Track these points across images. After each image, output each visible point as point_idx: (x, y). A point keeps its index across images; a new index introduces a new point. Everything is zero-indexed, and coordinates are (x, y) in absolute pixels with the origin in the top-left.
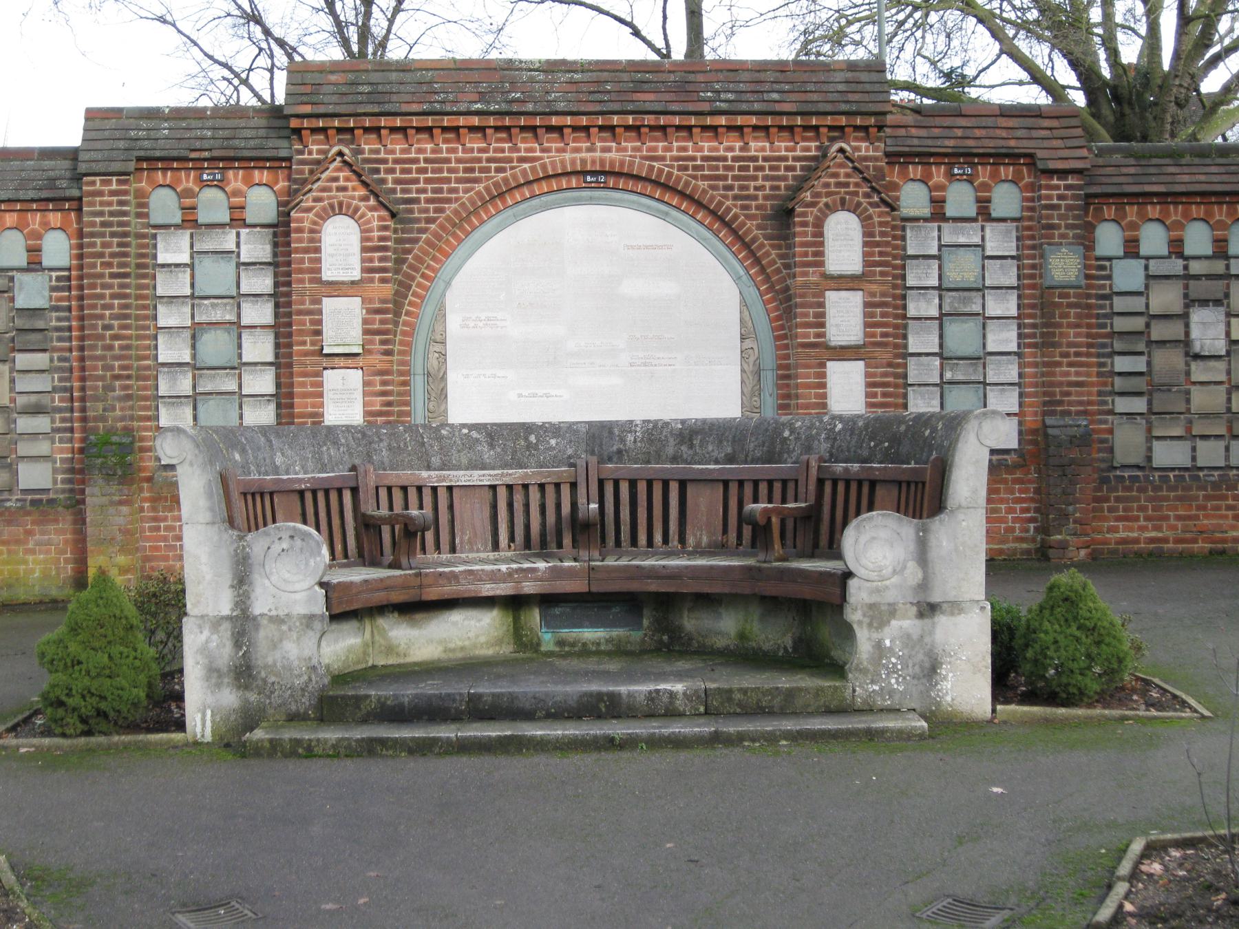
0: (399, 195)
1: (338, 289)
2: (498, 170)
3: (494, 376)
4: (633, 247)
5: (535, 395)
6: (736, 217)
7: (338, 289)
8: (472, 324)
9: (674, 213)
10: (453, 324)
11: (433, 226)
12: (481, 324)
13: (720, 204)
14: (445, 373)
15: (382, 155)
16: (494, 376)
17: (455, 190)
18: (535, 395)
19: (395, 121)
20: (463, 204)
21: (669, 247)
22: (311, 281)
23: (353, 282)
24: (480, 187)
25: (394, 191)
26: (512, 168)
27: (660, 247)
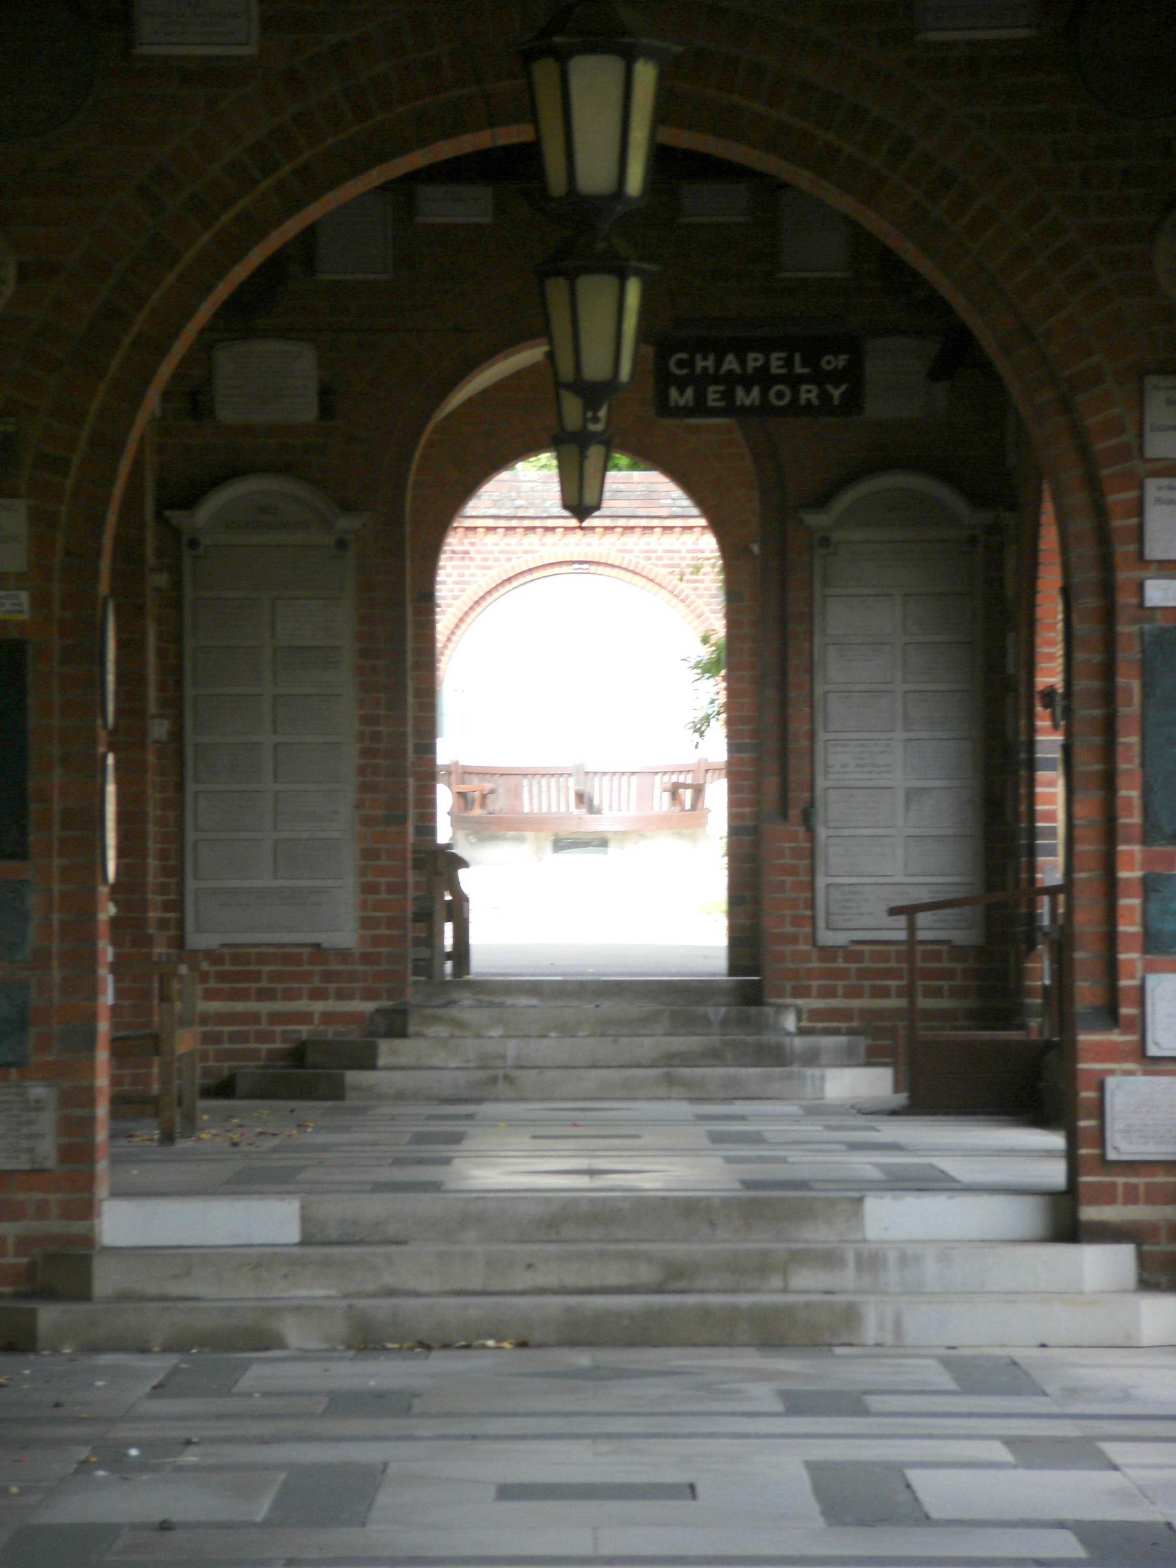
2: (509, 560)
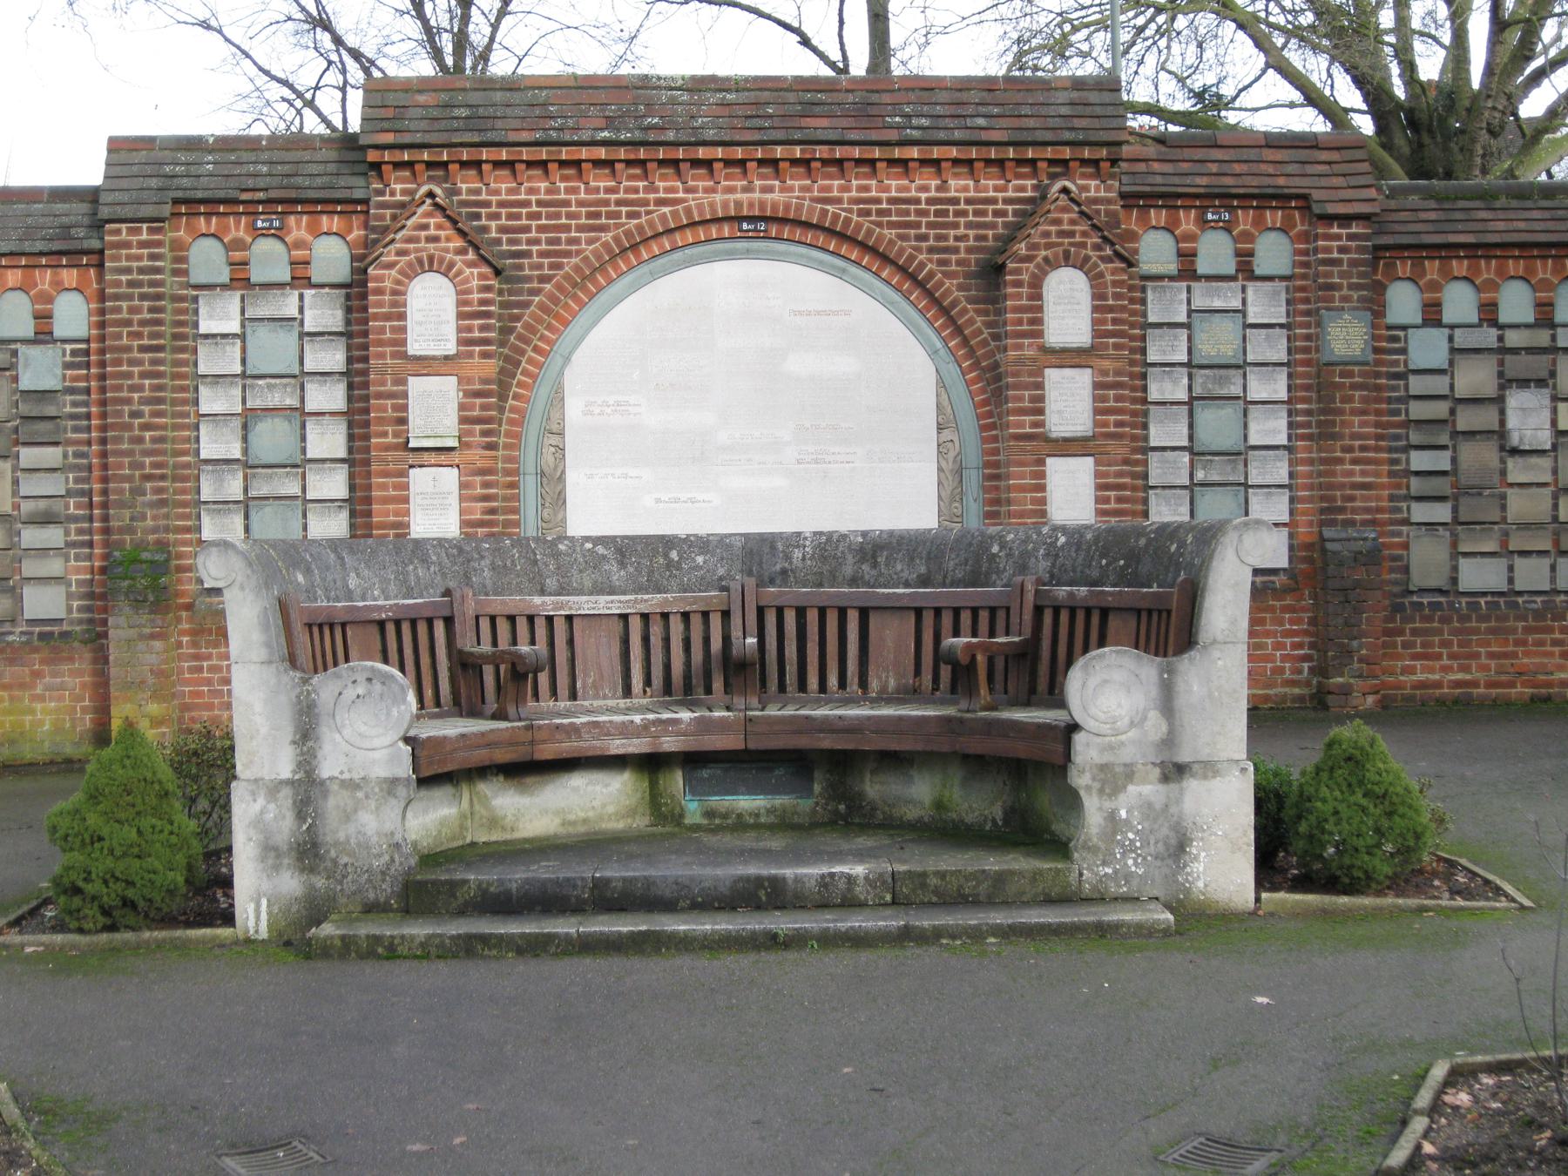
0: (505, 247)
1: (428, 365)
2: (630, 215)
3: (626, 476)
4: (800, 313)
5: (677, 500)
6: (931, 275)
7: (428, 365)
8: (597, 411)
9: (853, 269)
10: (574, 410)
11: (548, 286)
12: (609, 410)
13: (911, 258)
14: (563, 472)
15: (484, 197)
16: (626, 476)
17: (576, 241)
18: (677, 500)
20: (586, 258)
21: (847, 313)
22: (394, 355)
23: (446, 358)
24: (607, 237)
25: (498, 242)
26: (648, 213)
27: (836, 313)
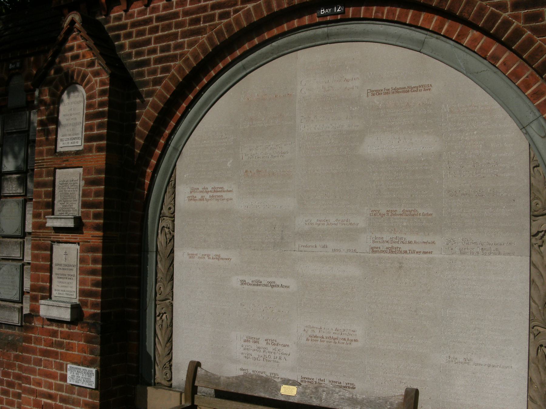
0: (134, 59)
1: (69, 159)
2: (223, 16)
3: (218, 258)
4: (378, 92)
5: (258, 283)
6: (518, 33)
7: (69, 159)
8: (198, 196)
9: (433, 41)
10: (183, 193)
11: (158, 87)
12: (207, 196)
13: (494, 17)
14: (172, 251)
15: (123, 21)
16: (218, 258)
17: (179, 46)
18: (258, 283)
19: (288, 27)
20: (188, 59)
21: (427, 88)
22: (49, 152)
23: (77, 153)
24: (203, 38)
25: (129, 55)
26: (236, 11)
27: (405, 90)
